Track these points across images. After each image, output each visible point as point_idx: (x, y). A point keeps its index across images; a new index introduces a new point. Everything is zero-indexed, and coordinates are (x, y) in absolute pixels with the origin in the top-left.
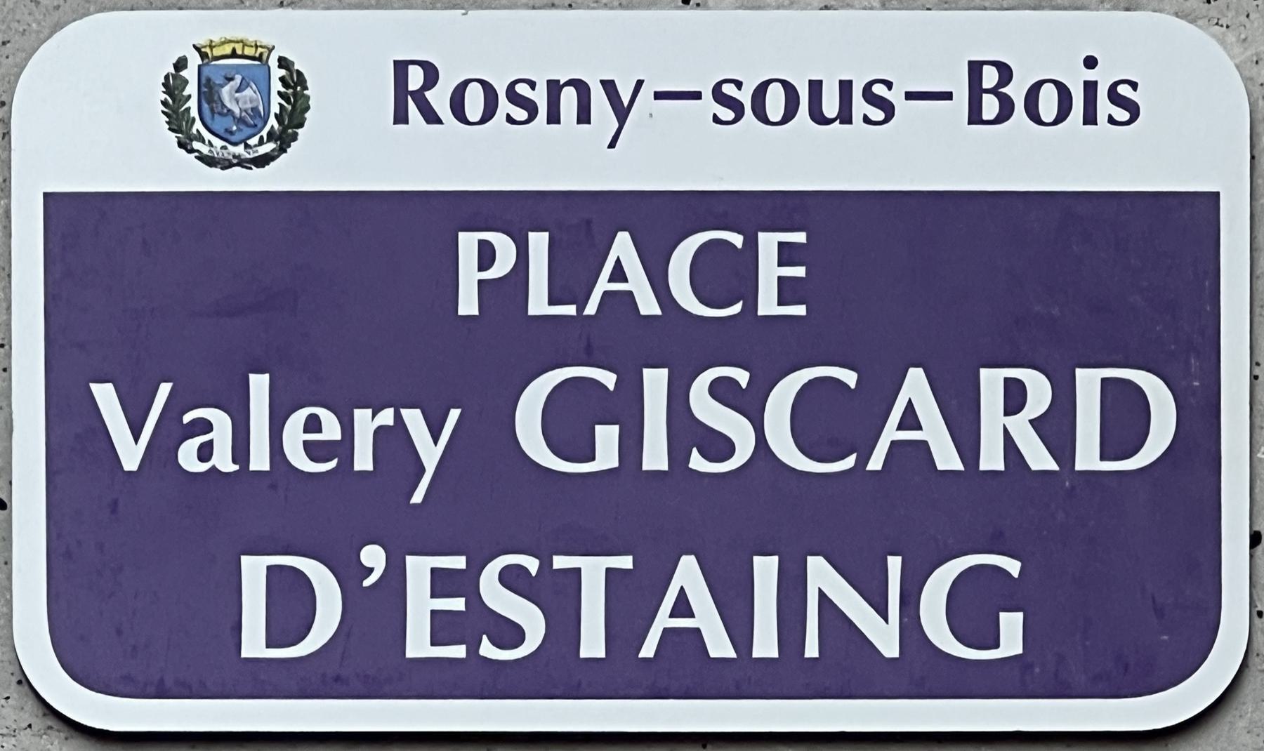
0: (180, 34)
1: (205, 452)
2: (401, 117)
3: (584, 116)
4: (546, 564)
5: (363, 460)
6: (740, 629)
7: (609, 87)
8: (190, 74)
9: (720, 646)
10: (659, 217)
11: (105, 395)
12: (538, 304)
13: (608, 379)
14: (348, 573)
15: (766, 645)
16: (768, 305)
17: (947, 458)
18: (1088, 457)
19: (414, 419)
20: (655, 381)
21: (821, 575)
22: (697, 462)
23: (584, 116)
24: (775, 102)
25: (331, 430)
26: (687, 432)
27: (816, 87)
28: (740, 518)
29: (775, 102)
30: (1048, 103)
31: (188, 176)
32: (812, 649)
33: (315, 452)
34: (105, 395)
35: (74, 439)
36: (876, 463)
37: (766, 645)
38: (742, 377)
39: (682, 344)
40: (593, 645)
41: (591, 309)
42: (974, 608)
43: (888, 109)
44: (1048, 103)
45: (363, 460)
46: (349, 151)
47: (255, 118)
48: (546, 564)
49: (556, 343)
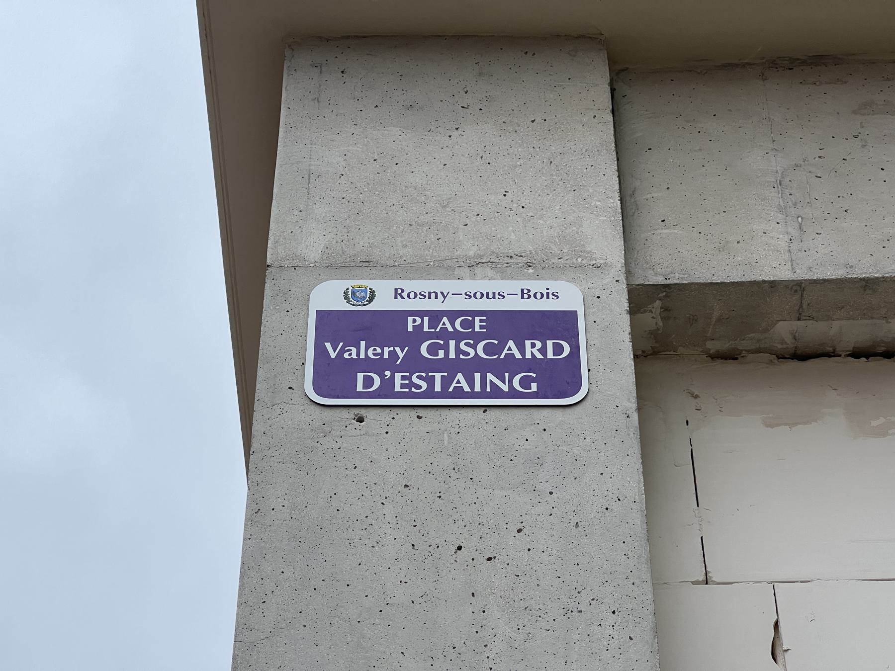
0: (348, 284)
1: (350, 355)
2: (396, 297)
3: (436, 297)
4: (427, 375)
5: (386, 356)
6: (471, 384)
7: (442, 293)
8: (350, 291)
9: (467, 389)
10: (452, 315)
11: (328, 345)
12: (426, 329)
13: (442, 342)
14: (382, 376)
15: (478, 388)
16: (477, 329)
17: (518, 356)
18: (550, 355)
19: (398, 349)
20: (452, 343)
21: (490, 376)
22: (461, 356)
23: (436, 297)
24: (478, 295)
25: (379, 350)
26: (458, 351)
27: (487, 293)
28: (470, 367)
29: (478, 295)
30: (539, 296)
31: (349, 307)
32: (488, 390)
33: (374, 354)
34: (328, 345)
35: (320, 352)
36: (502, 357)
37: (478, 388)
38: (472, 342)
39: (458, 337)
40: (438, 388)
41: (438, 330)
42: (525, 383)
43: (504, 297)
44: (539, 296)
45: (386, 356)
46: (384, 302)
47: (364, 298)
48: (427, 375)
49: (429, 336)
